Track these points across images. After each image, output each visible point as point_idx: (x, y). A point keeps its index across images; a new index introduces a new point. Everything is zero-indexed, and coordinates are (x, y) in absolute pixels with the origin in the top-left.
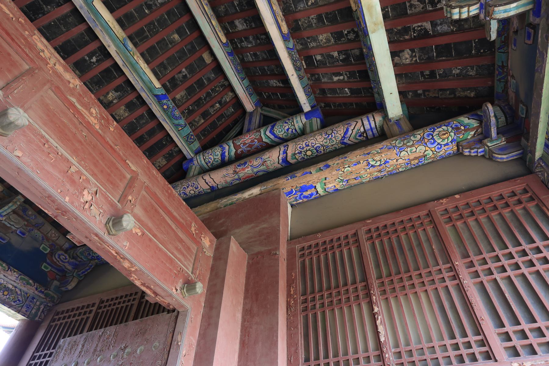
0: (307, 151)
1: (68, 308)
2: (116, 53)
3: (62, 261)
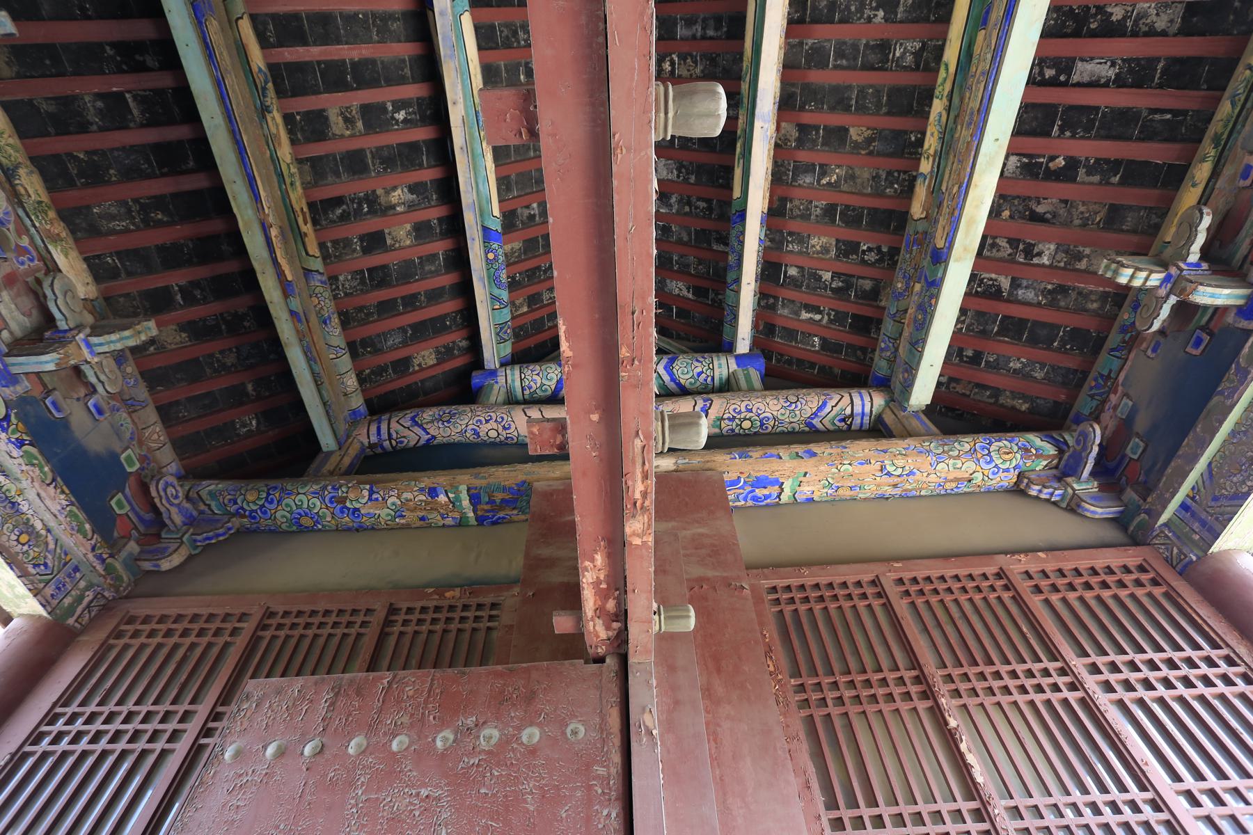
0: (745, 419)
1: (165, 612)
2: (460, 121)
3: (168, 499)
